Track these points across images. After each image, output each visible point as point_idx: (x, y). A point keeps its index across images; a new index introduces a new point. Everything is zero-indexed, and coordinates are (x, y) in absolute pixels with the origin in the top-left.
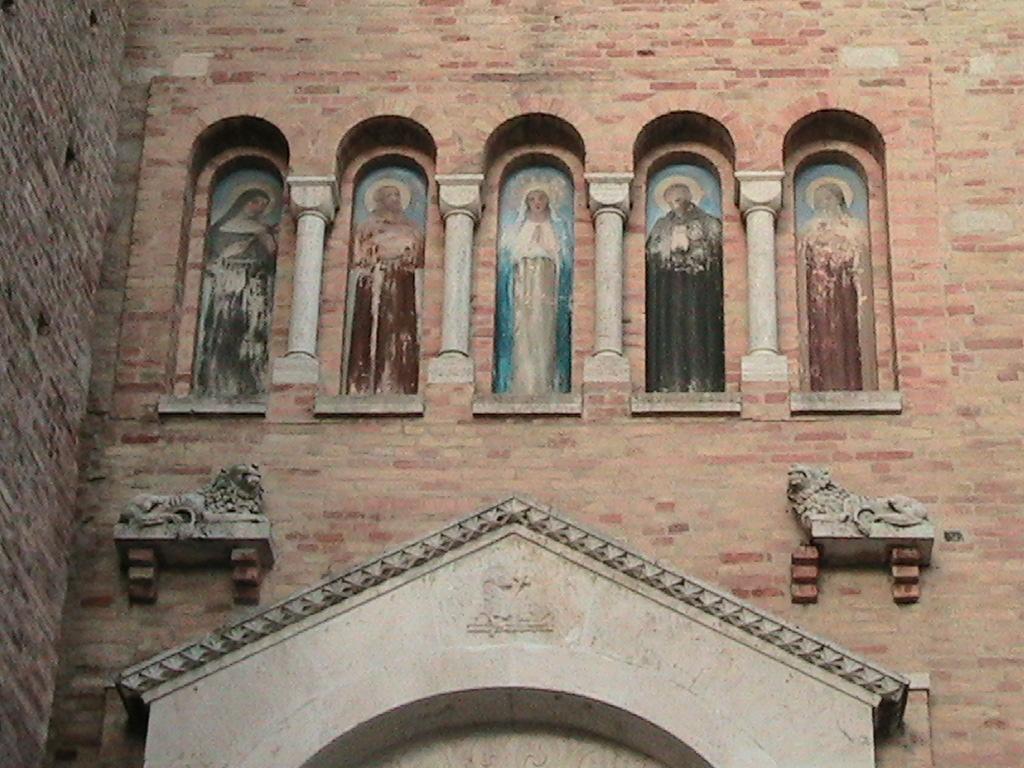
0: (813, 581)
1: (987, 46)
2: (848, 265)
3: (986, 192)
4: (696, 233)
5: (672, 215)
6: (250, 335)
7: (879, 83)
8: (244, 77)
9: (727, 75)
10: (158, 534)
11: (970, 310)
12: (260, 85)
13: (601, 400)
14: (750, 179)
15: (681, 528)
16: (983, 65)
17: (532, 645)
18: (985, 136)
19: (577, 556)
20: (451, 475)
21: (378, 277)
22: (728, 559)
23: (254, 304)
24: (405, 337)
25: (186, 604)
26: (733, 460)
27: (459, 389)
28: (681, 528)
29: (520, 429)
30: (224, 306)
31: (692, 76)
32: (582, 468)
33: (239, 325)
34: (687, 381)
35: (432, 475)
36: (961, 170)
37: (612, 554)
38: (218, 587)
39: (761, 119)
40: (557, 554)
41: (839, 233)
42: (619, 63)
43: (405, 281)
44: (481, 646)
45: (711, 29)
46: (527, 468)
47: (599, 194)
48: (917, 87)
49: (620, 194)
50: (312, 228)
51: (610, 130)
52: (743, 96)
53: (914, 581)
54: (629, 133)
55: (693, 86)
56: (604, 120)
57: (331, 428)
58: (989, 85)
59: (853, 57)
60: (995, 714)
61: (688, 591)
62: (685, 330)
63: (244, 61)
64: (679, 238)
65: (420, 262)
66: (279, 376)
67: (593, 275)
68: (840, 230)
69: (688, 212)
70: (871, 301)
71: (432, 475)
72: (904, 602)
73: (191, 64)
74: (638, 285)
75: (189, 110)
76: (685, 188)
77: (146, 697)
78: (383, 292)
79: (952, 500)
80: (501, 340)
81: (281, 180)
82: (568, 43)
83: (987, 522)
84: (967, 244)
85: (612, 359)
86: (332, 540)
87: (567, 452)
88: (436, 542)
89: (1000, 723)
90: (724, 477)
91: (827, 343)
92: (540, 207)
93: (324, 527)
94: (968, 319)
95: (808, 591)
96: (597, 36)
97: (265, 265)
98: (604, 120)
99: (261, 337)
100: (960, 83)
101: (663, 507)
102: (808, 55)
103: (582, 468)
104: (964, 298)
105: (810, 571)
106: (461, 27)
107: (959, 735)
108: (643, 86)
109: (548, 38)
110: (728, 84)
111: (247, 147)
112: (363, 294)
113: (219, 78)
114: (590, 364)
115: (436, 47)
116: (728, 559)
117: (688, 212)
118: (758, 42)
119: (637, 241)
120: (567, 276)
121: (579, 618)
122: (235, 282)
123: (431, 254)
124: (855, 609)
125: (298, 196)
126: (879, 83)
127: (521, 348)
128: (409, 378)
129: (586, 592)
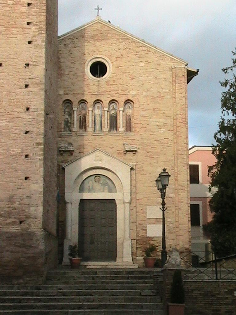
0: (126, 153)
1: (145, 91)
2: (130, 115)
3: (144, 110)
4: (115, 111)
5: (112, 109)
6: (69, 123)
7: (134, 96)
8: (67, 94)
9: (118, 95)
10: (64, 149)
11: (141, 123)
12: (69, 95)
13: (105, 133)
14: (120, 108)
15: (113, 147)
16: (144, 94)
17: (100, 162)
18: (144, 102)
19: (104, 153)
20: (91, 141)
21: (82, 116)
22: (118, 150)
23: (69, 119)
24: (85, 123)
25: (66, 156)
26: (118, 140)
27: (91, 132)
28: (113, 147)
29: (98, 136)
30: (66, 119)
31: (114, 95)
32: (104, 141)
33: (68, 122)
34: (114, 128)
35: (89, 141)
36: (142, 107)
37: (107, 153)
38: (69, 154)
39: (122, 100)
40: (124, 217)
41: (129, 111)
42: (107, 93)
43: (85, 117)
44: (95, 162)
45: (116, 88)
46: (98, 140)
47: (105, 109)
48: (137, 97)
49: (107, 109)
50: (75, 112)
51: (106, 101)
52: (120, 97)
53: (135, 153)
54: (108, 102)
55: (114, 96)
56: (105, 100)
57: (79, 136)
58: (145, 96)
59: (131, 92)
60: (141, 166)
61: (114, 157)
62: (113, 123)
63: (68, 92)
64: (113, 112)
65: (86, 114)
66: (74, 130)
67: (104, 117)
68: (129, 111)
69: (114, 109)
70: (132, 120)
71: (89, 141)
72: (134, 155)
73: (61, 92)
74: (109, 118)
75: (62, 98)
76: (113, 106)
77: (65, 167)
78: (83, 118)
79: (139, 144)
80: (95, 124)
81: (71, 105)
82: (101, 90)
83: (142, 147)
84: (142, 116)
85: (106, 128)
86: (79, 149)
87: (102, 139)
88: (90, 152)
89: (142, 167)
90: (118, 140)
91: (128, 124)
92: (98, 108)
93: (78, 147)
94: (141, 124)
95: (125, 154)
96: (105, 89)
97: (70, 114)
98: (105, 100)
99: (70, 123)
100: (142, 96)
101: (111, 145)
102: (126, 92)
103: (104, 141)
104: (141, 122)
105: (125, 153)
106: (90, 88)
107: (138, 168)
108: (109, 96)
109: (99, 89)
110: (118, 96)
111: (68, 102)
112: (80, 118)
113: (65, 94)
114: (104, 129)
115: (87, 90)
116: (118, 150)
117: (114, 109)
118: (121, 90)
119: (109, 113)
120: (101, 116)
121: (104, 159)
122: (67, 117)
123: (87, 114)
124: (130, 155)
125: (74, 109)
126: (134, 96)
127: (97, 125)
128: (86, 128)
129: (104, 157)
